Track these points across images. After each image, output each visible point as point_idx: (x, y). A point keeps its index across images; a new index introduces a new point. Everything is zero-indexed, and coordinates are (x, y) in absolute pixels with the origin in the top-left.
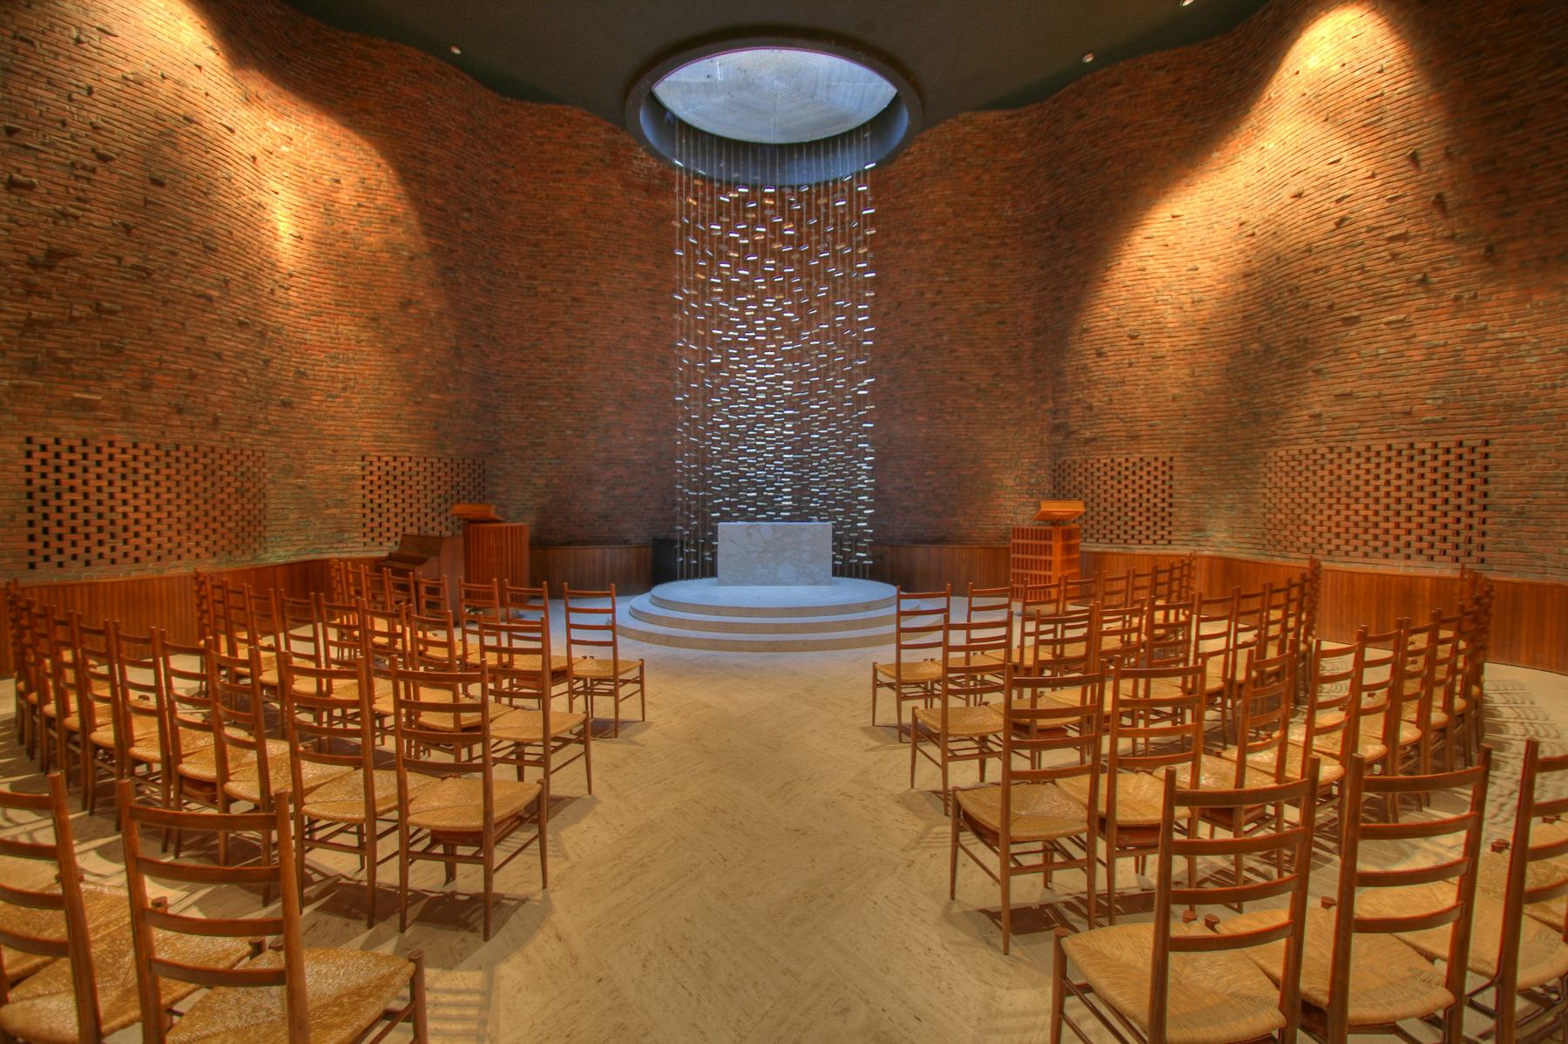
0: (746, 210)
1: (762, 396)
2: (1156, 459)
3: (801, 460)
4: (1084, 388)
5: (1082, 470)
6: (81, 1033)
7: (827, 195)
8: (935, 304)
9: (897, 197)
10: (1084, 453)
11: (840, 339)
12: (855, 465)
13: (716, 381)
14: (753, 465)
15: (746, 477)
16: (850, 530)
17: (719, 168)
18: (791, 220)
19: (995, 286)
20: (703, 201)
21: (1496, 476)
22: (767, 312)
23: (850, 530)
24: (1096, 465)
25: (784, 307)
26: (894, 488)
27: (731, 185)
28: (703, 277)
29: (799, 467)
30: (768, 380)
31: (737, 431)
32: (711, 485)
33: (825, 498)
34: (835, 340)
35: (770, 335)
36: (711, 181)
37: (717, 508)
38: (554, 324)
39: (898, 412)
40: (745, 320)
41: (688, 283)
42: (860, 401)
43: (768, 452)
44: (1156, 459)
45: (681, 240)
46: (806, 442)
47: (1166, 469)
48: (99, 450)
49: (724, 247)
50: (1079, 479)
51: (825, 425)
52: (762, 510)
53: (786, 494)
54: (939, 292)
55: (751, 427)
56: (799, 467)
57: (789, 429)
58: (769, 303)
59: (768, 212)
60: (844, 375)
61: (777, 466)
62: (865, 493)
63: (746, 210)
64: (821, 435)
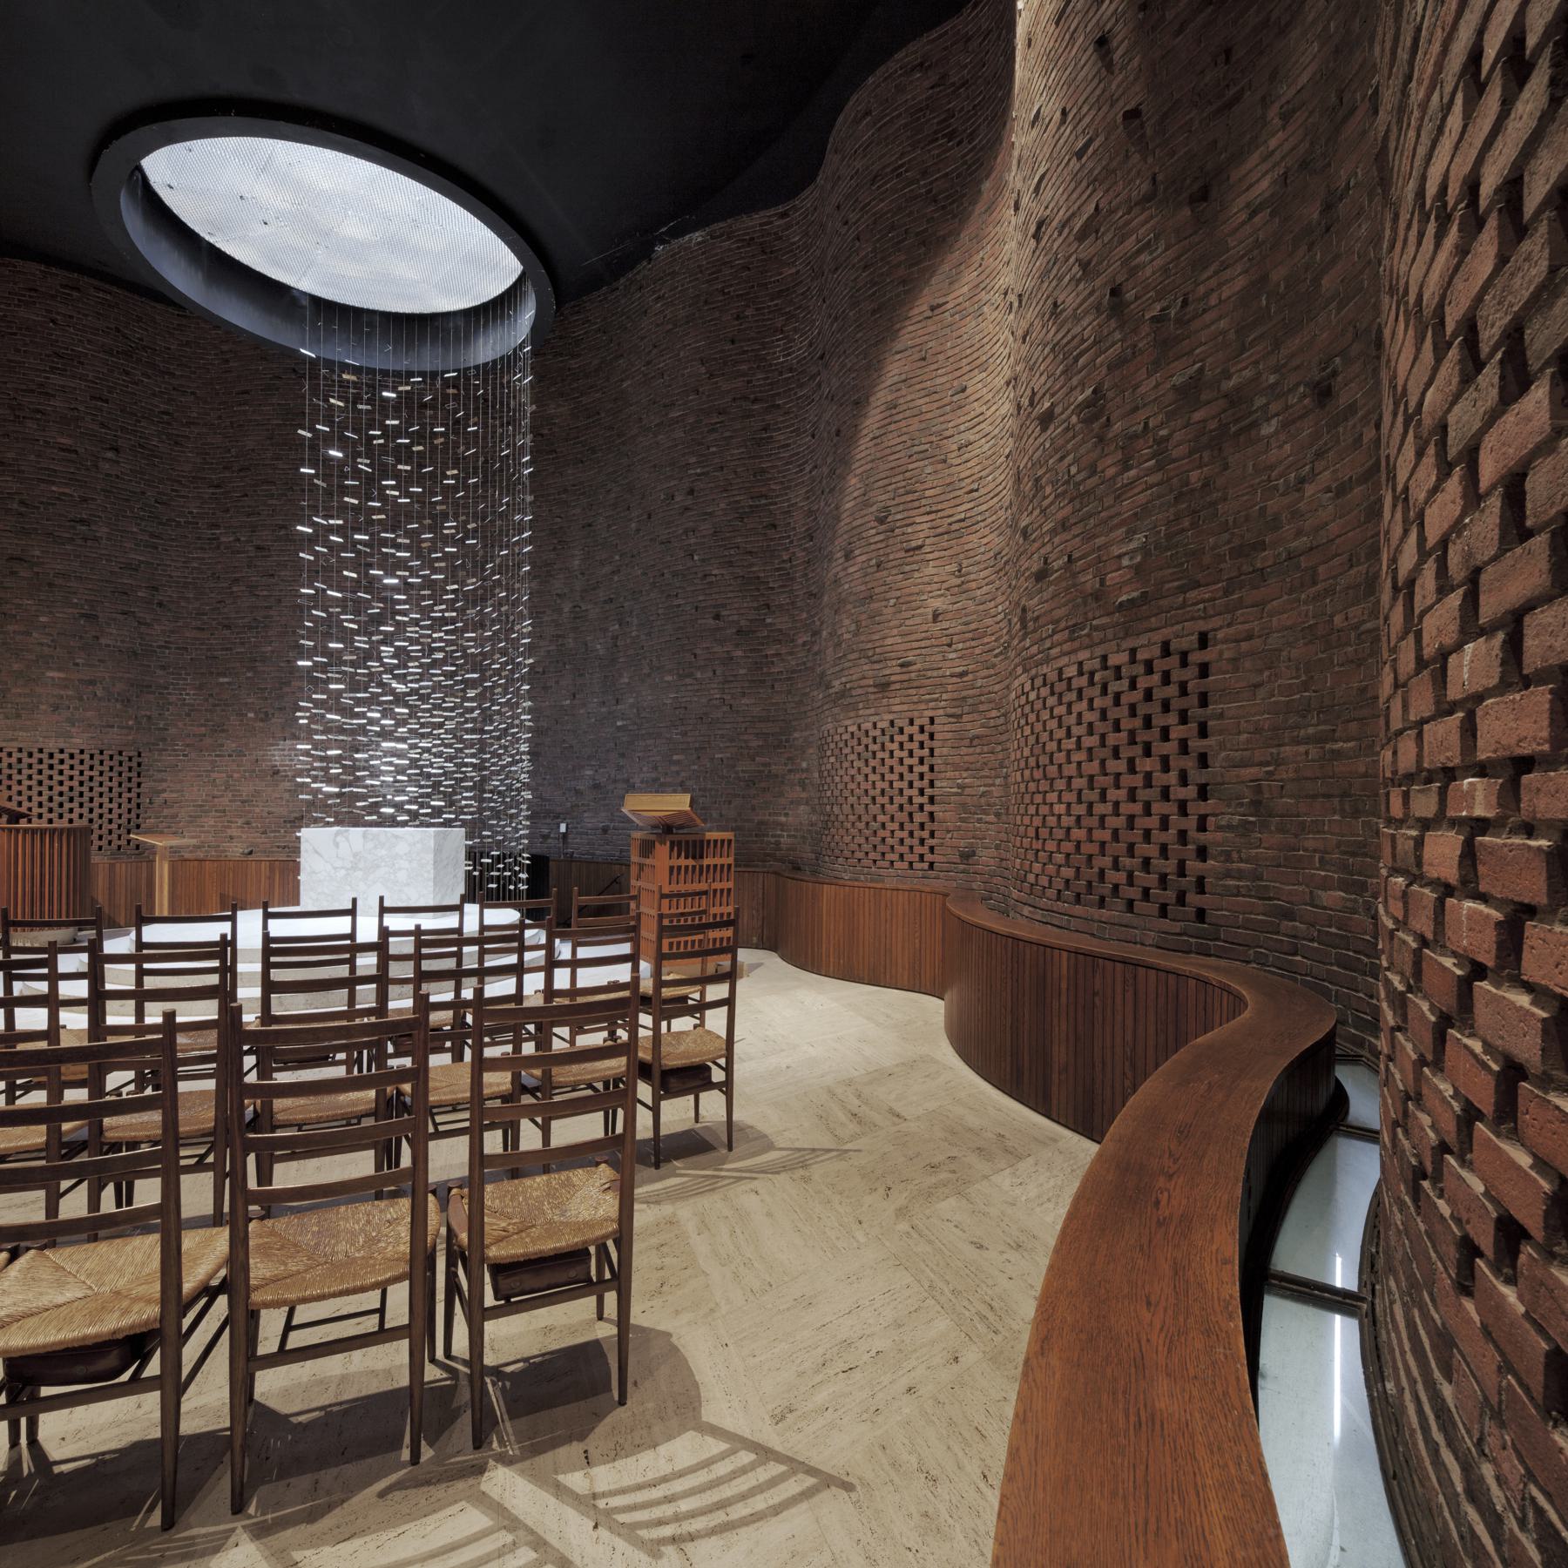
1: (440, 655)
2: (911, 723)
6: (1262, 1299)
8: (687, 509)
14: (428, 750)
17: (383, 357)
21: (1221, 716)
22: (447, 540)
30: (447, 633)
38: (236, 580)
39: (646, 670)
44: (911, 723)
47: (925, 737)
48: (30, 755)
54: (691, 492)
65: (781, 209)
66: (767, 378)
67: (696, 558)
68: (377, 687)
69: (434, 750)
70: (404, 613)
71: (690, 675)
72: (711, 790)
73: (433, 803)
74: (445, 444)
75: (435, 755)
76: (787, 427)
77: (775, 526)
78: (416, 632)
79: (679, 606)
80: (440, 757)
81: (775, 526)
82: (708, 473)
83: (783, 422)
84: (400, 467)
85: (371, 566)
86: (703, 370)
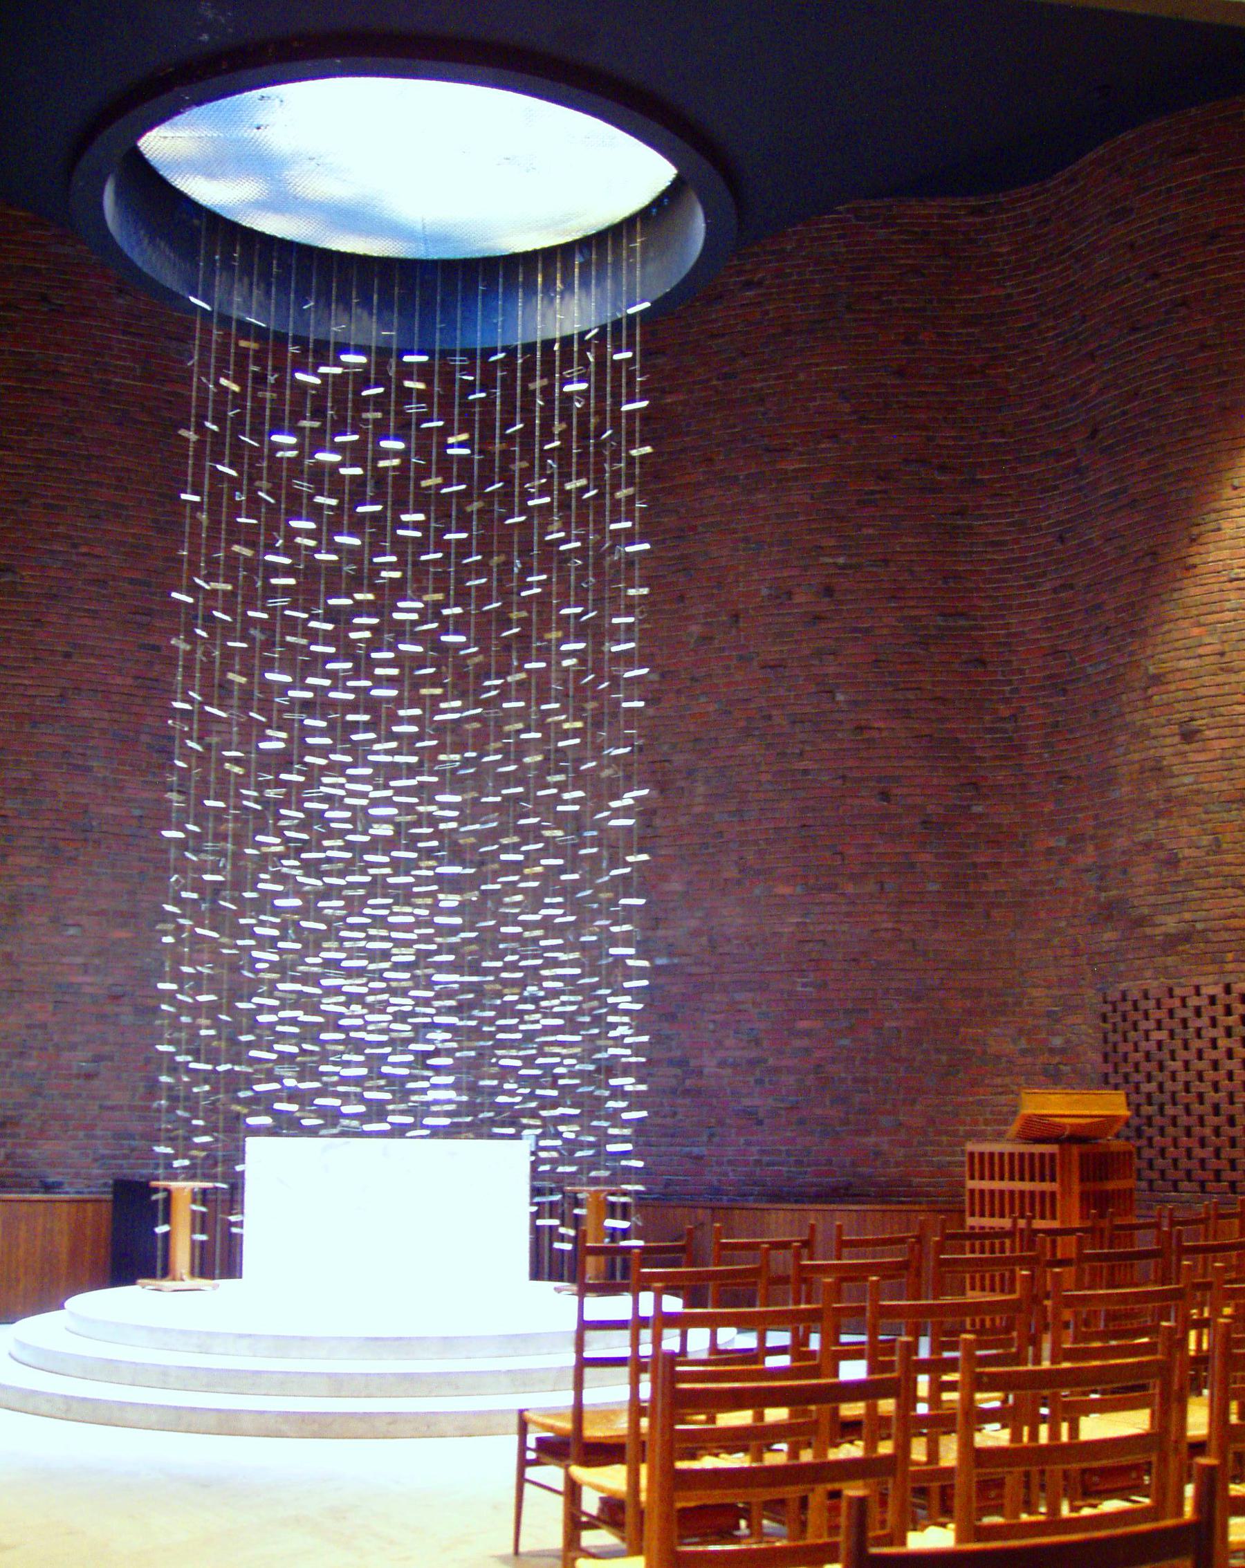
0: (363, 404)
1: (386, 830)
3: (476, 988)
4: (1159, 814)
5: (1162, 1014)
7: (548, 373)
8: (818, 618)
9: (723, 377)
10: (1165, 971)
11: (575, 699)
12: (602, 998)
13: (271, 793)
14: (358, 998)
15: (339, 1028)
16: (593, 1164)
18: (466, 426)
19: (957, 576)
20: (260, 379)
22: (401, 631)
23: (593, 1164)
24: (1193, 1002)
25: (444, 621)
26: (722, 1064)
27: (323, 352)
28: (248, 552)
29: (471, 1005)
30: (399, 791)
31: (320, 917)
32: (250, 1045)
33: (534, 1081)
34: (563, 697)
35: (409, 685)
36: (281, 340)
37: (262, 1103)
40: (347, 650)
41: (212, 562)
42: (615, 845)
43: (397, 967)
45: (199, 467)
46: (489, 943)
49: (304, 486)
50: (1156, 1036)
51: (535, 900)
52: (377, 1111)
53: (437, 1070)
55: (354, 906)
56: (471, 1005)
57: (451, 912)
58: (407, 611)
59: (413, 409)
60: (579, 780)
61: (419, 1001)
62: (626, 1070)
63: (363, 404)
64: (526, 925)
65: (973, 202)
66: (962, 438)
67: (840, 697)
68: (273, 881)
69: (370, 999)
70: (323, 751)
71: (832, 887)
72: (876, 1080)
73: (368, 1095)
74: (403, 469)
75: (372, 1008)
76: (999, 516)
77: (983, 663)
78: (342, 786)
79: (806, 772)
80: (383, 1012)
81: (983, 663)
82: (860, 566)
83: (989, 507)
84: (319, 499)
85: (269, 665)
86: (847, 408)
